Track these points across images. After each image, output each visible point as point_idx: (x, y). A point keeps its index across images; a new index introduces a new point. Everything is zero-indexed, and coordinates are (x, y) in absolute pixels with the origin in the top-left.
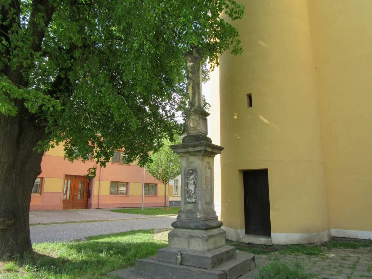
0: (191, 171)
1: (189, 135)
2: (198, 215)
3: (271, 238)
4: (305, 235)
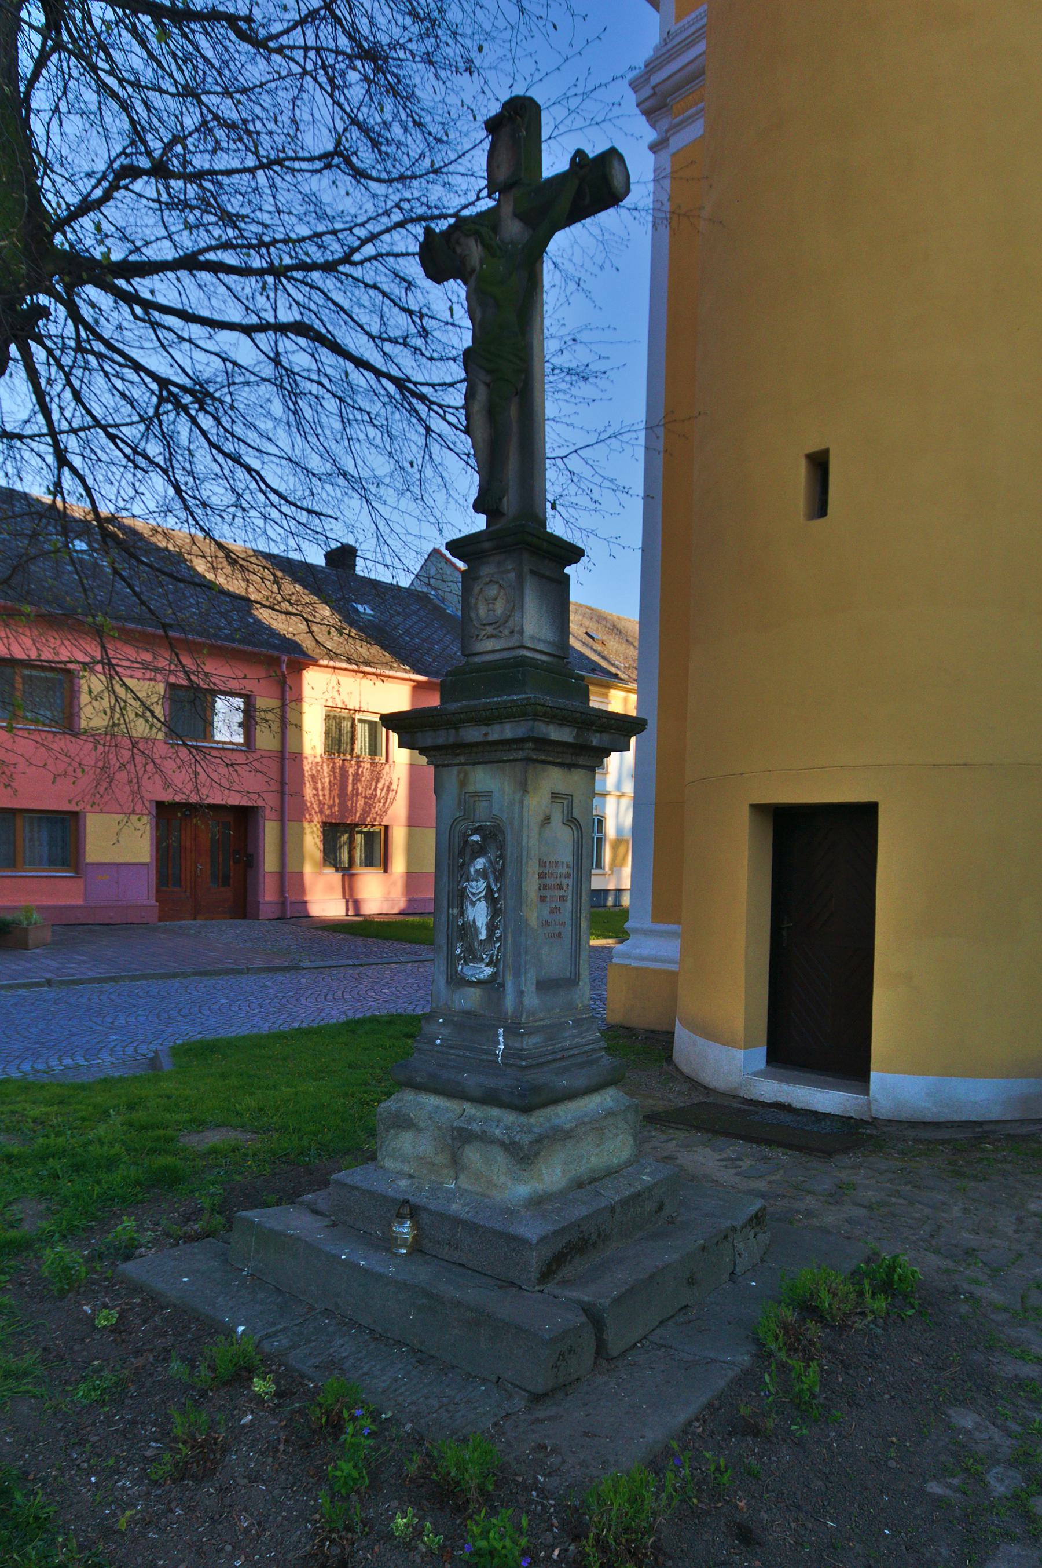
0: (476, 838)
1: (476, 659)
2: (501, 1039)
3: (866, 1091)
4: (1019, 1086)
